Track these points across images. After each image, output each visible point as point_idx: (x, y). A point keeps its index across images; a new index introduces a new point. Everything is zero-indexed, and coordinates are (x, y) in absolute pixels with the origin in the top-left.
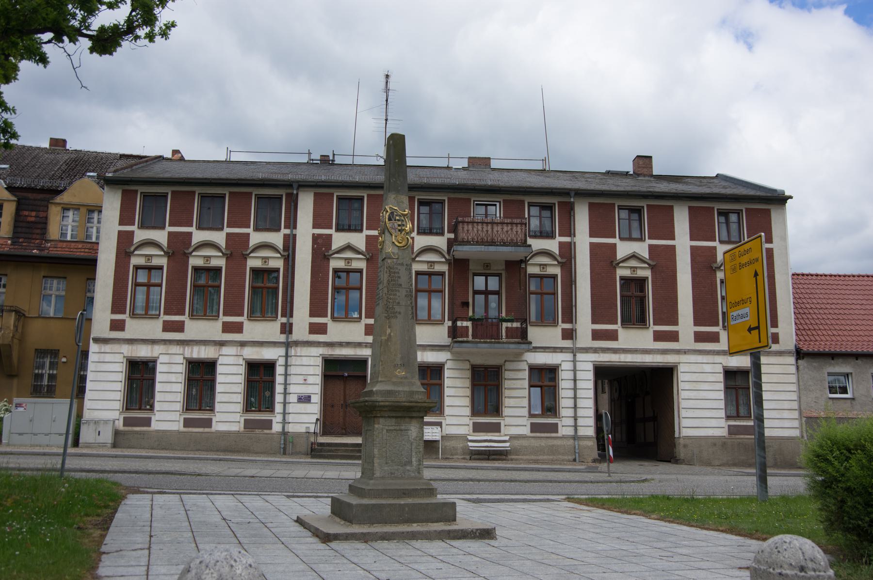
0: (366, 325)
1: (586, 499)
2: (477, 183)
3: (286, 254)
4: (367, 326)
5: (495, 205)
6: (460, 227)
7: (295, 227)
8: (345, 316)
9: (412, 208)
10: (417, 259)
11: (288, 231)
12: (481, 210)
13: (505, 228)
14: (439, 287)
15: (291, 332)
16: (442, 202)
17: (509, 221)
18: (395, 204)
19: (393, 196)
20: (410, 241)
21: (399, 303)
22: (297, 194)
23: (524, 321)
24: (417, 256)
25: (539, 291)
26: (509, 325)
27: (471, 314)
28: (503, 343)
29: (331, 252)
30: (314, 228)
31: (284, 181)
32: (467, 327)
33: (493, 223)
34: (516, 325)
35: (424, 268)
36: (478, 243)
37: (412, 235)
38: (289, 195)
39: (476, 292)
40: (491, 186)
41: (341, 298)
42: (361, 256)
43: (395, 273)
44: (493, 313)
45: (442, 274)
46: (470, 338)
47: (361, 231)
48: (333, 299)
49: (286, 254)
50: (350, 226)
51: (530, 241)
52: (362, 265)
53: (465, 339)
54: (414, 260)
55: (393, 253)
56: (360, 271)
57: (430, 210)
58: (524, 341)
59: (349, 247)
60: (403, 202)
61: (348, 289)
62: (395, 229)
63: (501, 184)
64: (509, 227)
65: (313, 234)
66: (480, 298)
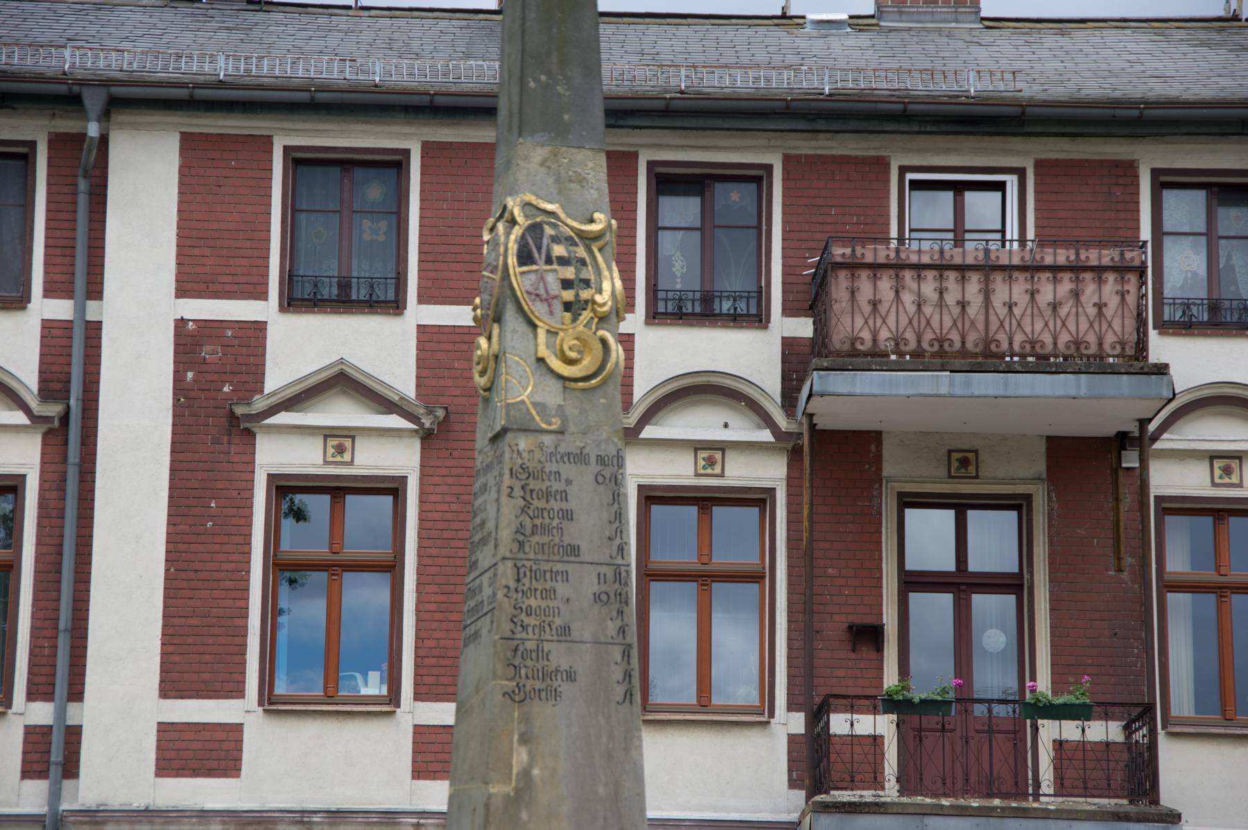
0: (419, 730)
1: (623, 280)
2: (917, 85)
3: (53, 410)
4: (422, 733)
5: (1001, 187)
6: (840, 286)
7: (95, 290)
8: (322, 689)
9: (622, 208)
10: (648, 432)
11: (61, 309)
12: (935, 211)
13: (1047, 293)
14: (748, 558)
15: (71, 768)
16: (757, 177)
17: (1063, 256)
18: (552, 186)
19: (539, 153)
20: (617, 351)
21: (566, 630)
22: (104, 141)
23: (1141, 713)
24: (648, 416)
25: (1210, 575)
26: (1070, 730)
27: (891, 679)
28: (1045, 814)
29: (259, 404)
30: (181, 292)
31: (40, 78)
32: (876, 740)
33: (988, 269)
34: (1103, 731)
35: (677, 471)
36: (920, 360)
37: (624, 328)
38: (66, 145)
39: (913, 582)
40: (980, 100)
41: (306, 610)
42: (395, 421)
43: (547, 495)
44: (993, 678)
45: (760, 499)
46: (891, 791)
47: (396, 306)
48: (272, 612)
49: (53, 410)
50: (345, 285)
51: (1161, 348)
52: (402, 459)
53: (868, 795)
54: (631, 435)
55: (541, 407)
56: (393, 488)
57: (706, 211)
58: (1143, 807)
59: (341, 381)
60: (581, 181)
61: (337, 567)
62: (548, 300)
63: (1028, 89)
64: (1066, 286)
65: (181, 323)
66: (935, 610)
